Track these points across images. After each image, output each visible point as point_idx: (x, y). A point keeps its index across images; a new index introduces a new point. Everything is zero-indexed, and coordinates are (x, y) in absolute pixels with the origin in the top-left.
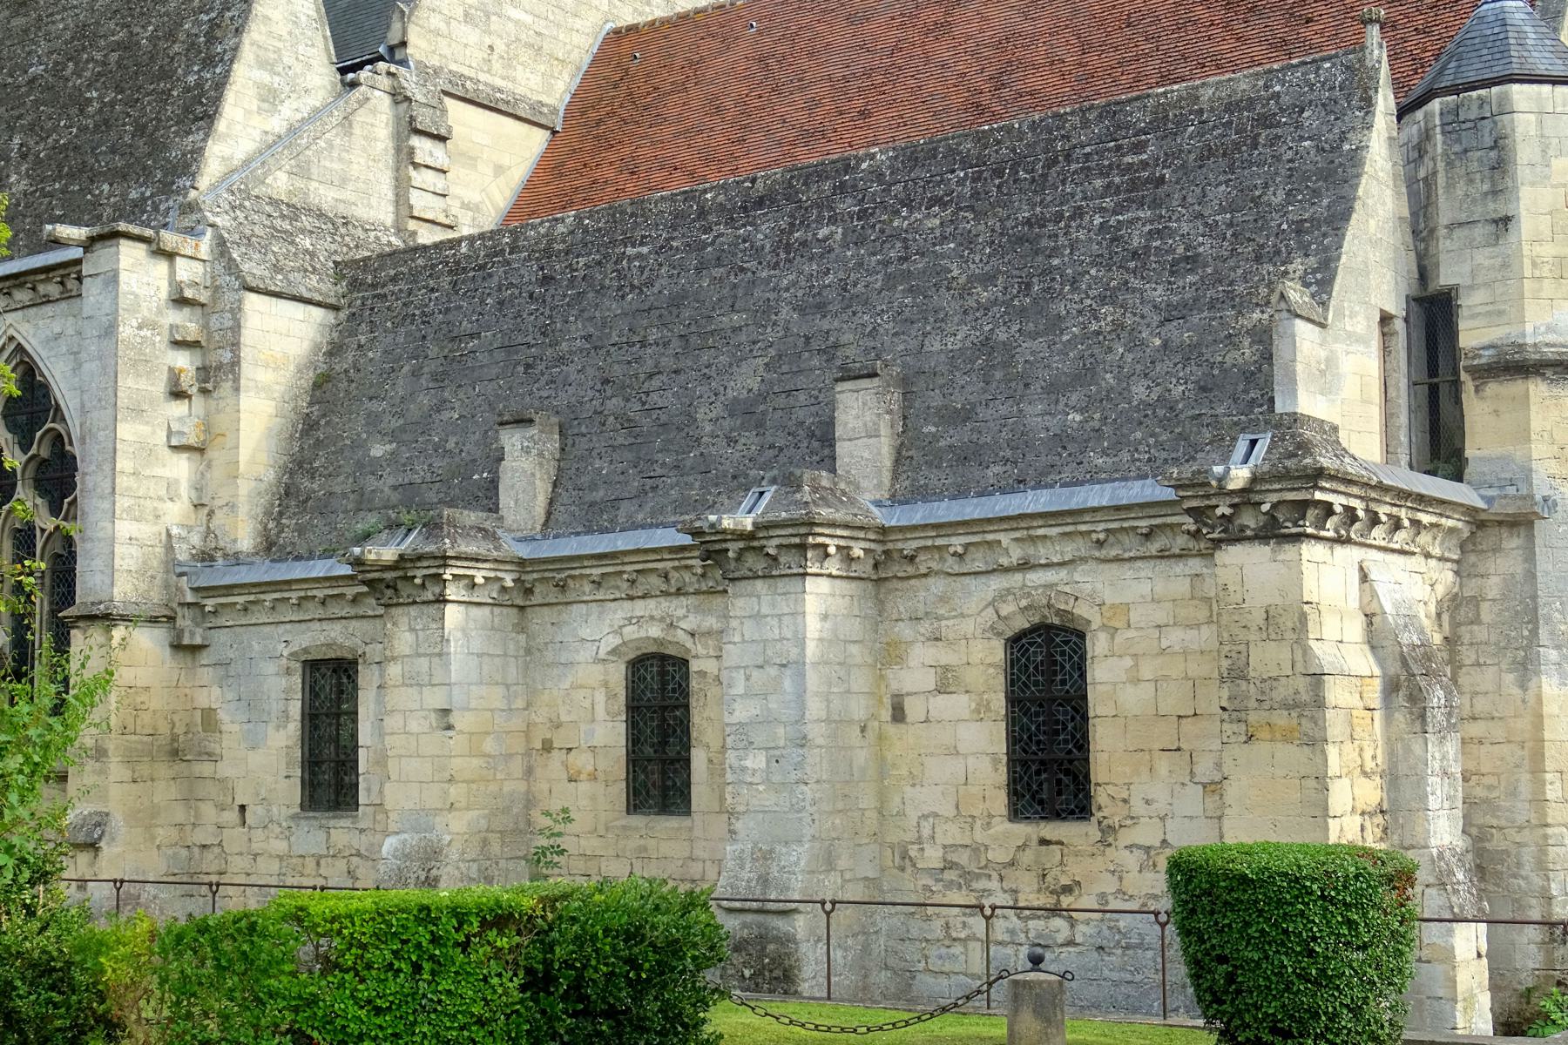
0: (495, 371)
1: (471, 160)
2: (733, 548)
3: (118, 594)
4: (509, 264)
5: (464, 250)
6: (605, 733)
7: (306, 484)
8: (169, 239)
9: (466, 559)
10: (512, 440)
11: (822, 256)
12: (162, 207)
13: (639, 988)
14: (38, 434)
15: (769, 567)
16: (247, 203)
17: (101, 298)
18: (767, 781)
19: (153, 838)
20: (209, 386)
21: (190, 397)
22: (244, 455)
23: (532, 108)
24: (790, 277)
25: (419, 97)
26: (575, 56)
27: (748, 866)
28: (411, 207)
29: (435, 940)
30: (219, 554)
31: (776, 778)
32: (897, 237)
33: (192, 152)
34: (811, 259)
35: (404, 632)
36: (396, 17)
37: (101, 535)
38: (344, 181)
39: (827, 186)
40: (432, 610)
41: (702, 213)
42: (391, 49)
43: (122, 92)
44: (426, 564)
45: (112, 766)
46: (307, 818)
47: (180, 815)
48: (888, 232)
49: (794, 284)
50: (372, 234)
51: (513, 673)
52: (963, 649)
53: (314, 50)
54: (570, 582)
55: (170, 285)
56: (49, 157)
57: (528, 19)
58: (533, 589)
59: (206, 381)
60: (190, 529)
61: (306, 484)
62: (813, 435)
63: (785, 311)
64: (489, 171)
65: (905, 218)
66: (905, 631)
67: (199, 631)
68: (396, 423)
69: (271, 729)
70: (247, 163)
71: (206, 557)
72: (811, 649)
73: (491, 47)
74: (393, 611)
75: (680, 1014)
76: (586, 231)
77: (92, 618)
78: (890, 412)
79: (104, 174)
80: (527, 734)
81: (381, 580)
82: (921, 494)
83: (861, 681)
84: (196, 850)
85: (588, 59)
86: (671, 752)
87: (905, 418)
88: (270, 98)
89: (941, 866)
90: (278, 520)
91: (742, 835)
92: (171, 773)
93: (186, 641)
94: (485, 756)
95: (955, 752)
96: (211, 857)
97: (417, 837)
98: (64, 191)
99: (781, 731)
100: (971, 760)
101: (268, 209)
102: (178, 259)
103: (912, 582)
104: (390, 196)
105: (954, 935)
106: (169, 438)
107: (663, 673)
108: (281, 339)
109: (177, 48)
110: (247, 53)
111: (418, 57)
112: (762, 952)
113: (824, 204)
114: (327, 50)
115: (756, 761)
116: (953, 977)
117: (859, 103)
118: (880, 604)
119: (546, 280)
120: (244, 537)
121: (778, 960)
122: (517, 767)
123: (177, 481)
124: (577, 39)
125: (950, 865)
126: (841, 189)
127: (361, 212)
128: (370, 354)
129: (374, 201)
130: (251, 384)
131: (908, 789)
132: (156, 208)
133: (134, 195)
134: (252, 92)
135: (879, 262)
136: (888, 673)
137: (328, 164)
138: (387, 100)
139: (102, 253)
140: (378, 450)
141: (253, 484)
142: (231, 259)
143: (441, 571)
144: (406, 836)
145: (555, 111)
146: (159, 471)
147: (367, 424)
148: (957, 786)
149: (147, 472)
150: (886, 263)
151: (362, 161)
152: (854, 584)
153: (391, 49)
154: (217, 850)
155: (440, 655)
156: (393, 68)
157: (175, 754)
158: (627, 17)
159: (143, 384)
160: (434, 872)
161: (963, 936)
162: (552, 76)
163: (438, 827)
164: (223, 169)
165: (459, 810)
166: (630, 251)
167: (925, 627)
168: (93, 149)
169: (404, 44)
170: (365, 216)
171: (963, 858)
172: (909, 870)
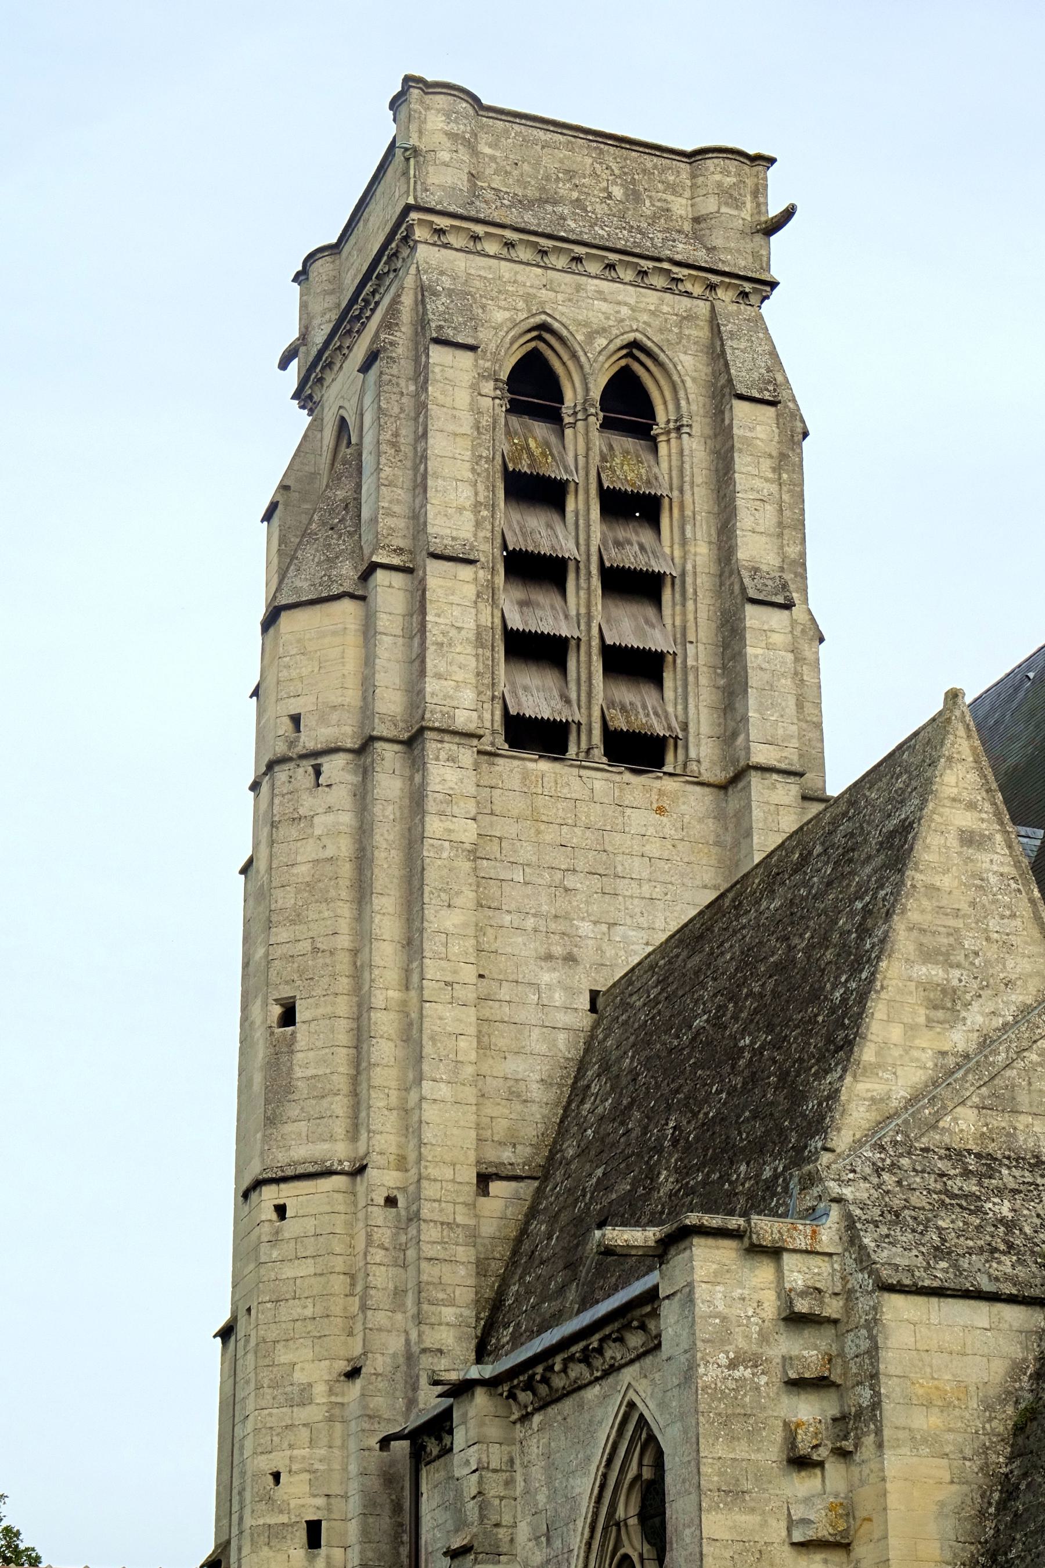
16: (905, 1162)
20: (848, 1445)
21: (820, 1464)
33: (828, 1098)
53: (1018, 922)
55: (779, 1297)
56: (697, 1139)
59: (846, 1438)
79: (743, 1150)
88: (946, 1003)
98: (705, 1183)
102: (786, 1256)
106: (789, 1530)
109: (829, 955)
110: (903, 938)
130: (902, 1435)
133: (767, 1173)
139: (677, 1260)
142: (862, 1248)
159: (742, 1451)
164: (874, 1116)
168: (739, 1116)
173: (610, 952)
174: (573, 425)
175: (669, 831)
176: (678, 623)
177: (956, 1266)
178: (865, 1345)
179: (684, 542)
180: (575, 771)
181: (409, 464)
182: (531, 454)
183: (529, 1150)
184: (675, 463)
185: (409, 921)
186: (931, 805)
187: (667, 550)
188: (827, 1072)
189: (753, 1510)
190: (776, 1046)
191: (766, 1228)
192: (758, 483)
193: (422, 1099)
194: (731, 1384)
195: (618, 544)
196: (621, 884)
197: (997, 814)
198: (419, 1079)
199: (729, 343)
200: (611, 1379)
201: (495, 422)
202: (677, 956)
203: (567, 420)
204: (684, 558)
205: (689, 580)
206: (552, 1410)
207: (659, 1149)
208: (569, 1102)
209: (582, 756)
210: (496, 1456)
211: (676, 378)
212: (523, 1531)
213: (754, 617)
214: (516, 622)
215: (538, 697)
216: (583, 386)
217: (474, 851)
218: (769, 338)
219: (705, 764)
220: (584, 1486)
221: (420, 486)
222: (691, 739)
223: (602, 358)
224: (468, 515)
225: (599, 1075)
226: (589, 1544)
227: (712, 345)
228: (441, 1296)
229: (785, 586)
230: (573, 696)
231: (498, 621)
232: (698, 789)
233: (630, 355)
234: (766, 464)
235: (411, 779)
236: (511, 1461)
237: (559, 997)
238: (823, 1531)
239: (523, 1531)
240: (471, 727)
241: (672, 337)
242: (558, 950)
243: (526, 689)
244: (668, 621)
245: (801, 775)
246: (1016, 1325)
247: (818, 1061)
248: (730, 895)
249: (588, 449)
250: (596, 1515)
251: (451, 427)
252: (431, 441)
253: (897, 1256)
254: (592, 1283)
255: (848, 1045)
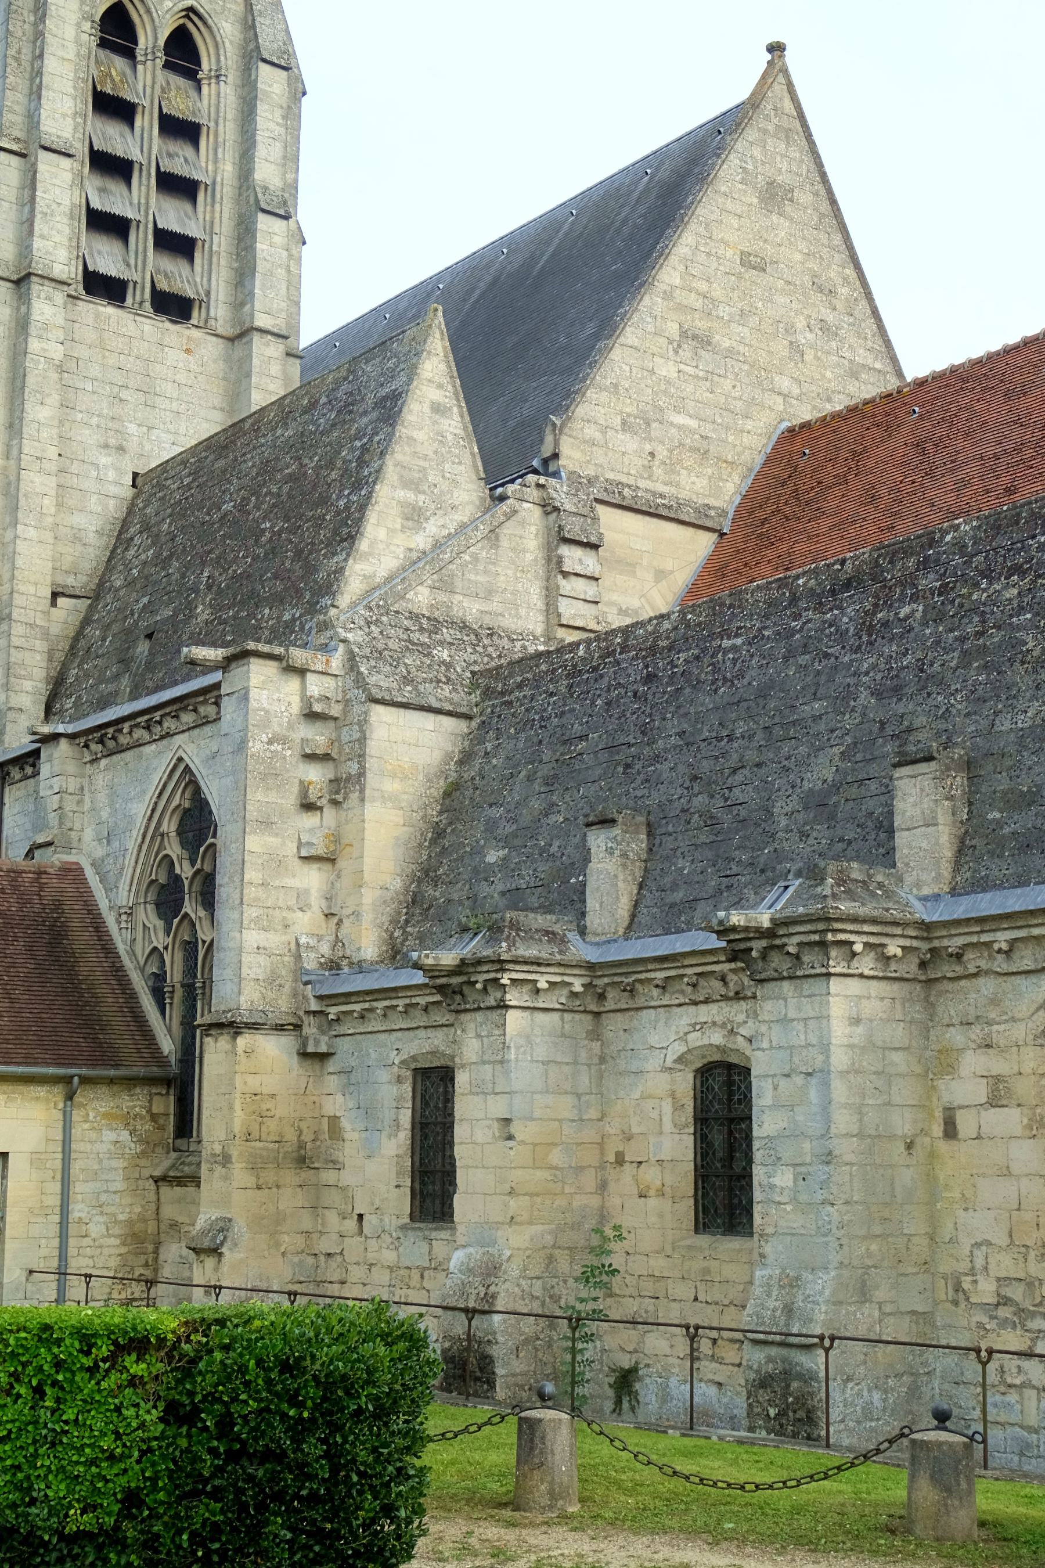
0: (598, 771)
1: (629, 566)
2: (757, 946)
3: (244, 1002)
4: (619, 664)
5: (581, 653)
6: (670, 1144)
7: (430, 892)
8: (298, 656)
9: (526, 963)
10: (598, 841)
11: (902, 637)
12: (307, 627)
13: (299, 1430)
14: (202, 849)
15: (794, 967)
16: (384, 619)
17: (235, 715)
18: (794, 1200)
19: (278, 1245)
20: (339, 798)
21: (321, 809)
22: (368, 862)
23: (697, 511)
24: (871, 660)
25: (568, 507)
26: (746, 457)
27: (775, 1293)
28: (559, 615)
29: (58, 1365)
30: (345, 962)
31: (803, 1197)
32: (974, 610)
33: (335, 572)
34: (891, 640)
35: (469, 1044)
36: (548, 429)
37: (231, 944)
38: (489, 593)
39: (911, 562)
40: (495, 1015)
41: (794, 600)
42: (546, 462)
43: (288, 521)
44: (485, 968)
45: (236, 1172)
46: (413, 1229)
47: (307, 1224)
48: (966, 607)
49: (874, 667)
50: (519, 644)
51: (584, 1081)
52: (1015, 1056)
53: (462, 468)
54: (638, 986)
55: (302, 700)
56: (228, 587)
57: (693, 423)
58: (606, 992)
59: (337, 793)
60: (320, 938)
61: (430, 892)
62: (881, 826)
63: (864, 695)
64: (650, 577)
65: (984, 590)
66: (956, 1037)
67: (324, 1039)
68: (510, 828)
69: (384, 1139)
70: (389, 579)
71: (333, 966)
72: (839, 1059)
73: (652, 454)
74: (465, 1017)
75: (354, 1461)
76: (688, 626)
77: (220, 1026)
78: (951, 798)
79: (266, 599)
80: (601, 1145)
81: (449, 985)
82: (981, 885)
83: (905, 1092)
84: (322, 1258)
85: (759, 460)
86: (737, 1168)
87: (971, 804)
88: (414, 517)
89: (994, 1301)
90: (403, 928)
91: (771, 1259)
92: (298, 1180)
93: (310, 1049)
94: (551, 1168)
95: (1006, 1173)
96: (334, 1265)
97: (481, 1251)
98: (235, 617)
99: (807, 1146)
100: (1024, 1181)
101: (407, 623)
102: (309, 675)
103: (963, 983)
104: (541, 605)
105: (1009, 1380)
107: (730, 1083)
108: (410, 749)
109: (334, 475)
110: (391, 471)
111: (571, 468)
112: (786, 1392)
113: (908, 581)
114: (475, 466)
115: (784, 1179)
116: (1009, 1429)
117: (1005, 480)
118: (930, 1006)
119: (650, 678)
120: (368, 944)
121: (802, 1400)
122: (589, 1180)
123: (307, 891)
124: (746, 440)
125: (1004, 1301)
126: (925, 565)
127: (509, 623)
128: (494, 761)
129: (523, 612)
130: (376, 794)
131: (961, 1213)
132: (302, 629)
133: (287, 617)
134: (395, 510)
135: (956, 639)
136: (940, 1084)
137: (473, 577)
138: (537, 511)
139: (237, 671)
140: (492, 857)
141: (379, 892)
142: (359, 673)
143: (499, 976)
144: (471, 1250)
145: (723, 513)
146: (289, 882)
147: (486, 830)
148: (1010, 1211)
149: (277, 883)
150: (962, 639)
151: (510, 573)
152: (896, 986)
153: (546, 462)
154: (339, 1259)
155: (502, 1062)
156: (542, 480)
157: (302, 1161)
158: (806, 414)
159: (273, 797)
160: (492, 1288)
161: (1017, 1382)
162: (721, 479)
163: (500, 1241)
164: (364, 587)
165: (520, 1224)
166: (726, 643)
167: (976, 1032)
168: (262, 576)
169: (556, 456)
170: (513, 627)
171: (1017, 1293)
172: (963, 1304)
173: (148, 447)
174: (144, 63)
175: (192, 367)
176: (208, 218)
177: (416, 689)
178: (357, 735)
179: (216, 161)
180: (132, 316)
181: (27, 76)
182: (113, 81)
183: (85, 578)
184: (213, 102)
185: (11, 411)
186: (415, 383)
187: (203, 165)
188: (334, 554)
189: (277, 835)
190: (289, 531)
191: (298, 656)
192: (272, 126)
193: (16, 537)
194: (268, 754)
195: (170, 155)
196: (158, 400)
197: (456, 393)
198: (15, 523)
199: (258, 19)
200: (165, 742)
201: (90, 53)
202: (206, 458)
203: (139, 58)
204: (215, 172)
205: (218, 188)
206: (116, 758)
207: (196, 591)
208: (115, 548)
209: (136, 306)
210: (72, 785)
211: (218, 38)
212: (89, 834)
213: (263, 222)
214: (96, 204)
215: (108, 258)
216: (152, 35)
217: (61, 366)
218: (285, 19)
219: (220, 322)
220: (140, 809)
221: (36, 93)
222: (212, 303)
223: (168, 16)
224: (69, 121)
225: (141, 532)
226: (140, 847)
227: (245, 18)
228: (23, 672)
229: (285, 203)
230: (132, 262)
231: (84, 201)
232: (214, 339)
233: (187, 16)
234: (278, 113)
235: (18, 309)
236: (82, 788)
237: (111, 475)
238: (321, 851)
239: (89, 834)
240: (64, 277)
241: (218, 8)
242: (112, 442)
243: (99, 253)
244: (201, 216)
245: (286, 338)
246: (449, 730)
247: (327, 546)
248: (250, 421)
249: (154, 83)
250: (147, 828)
251: (60, 53)
252: (46, 62)
253: (381, 681)
254: (143, 675)
255: (351, 539)
